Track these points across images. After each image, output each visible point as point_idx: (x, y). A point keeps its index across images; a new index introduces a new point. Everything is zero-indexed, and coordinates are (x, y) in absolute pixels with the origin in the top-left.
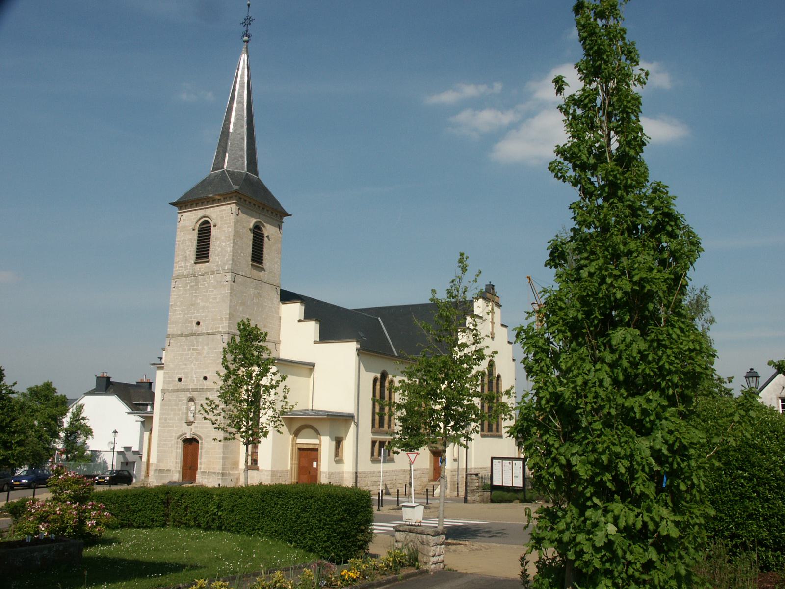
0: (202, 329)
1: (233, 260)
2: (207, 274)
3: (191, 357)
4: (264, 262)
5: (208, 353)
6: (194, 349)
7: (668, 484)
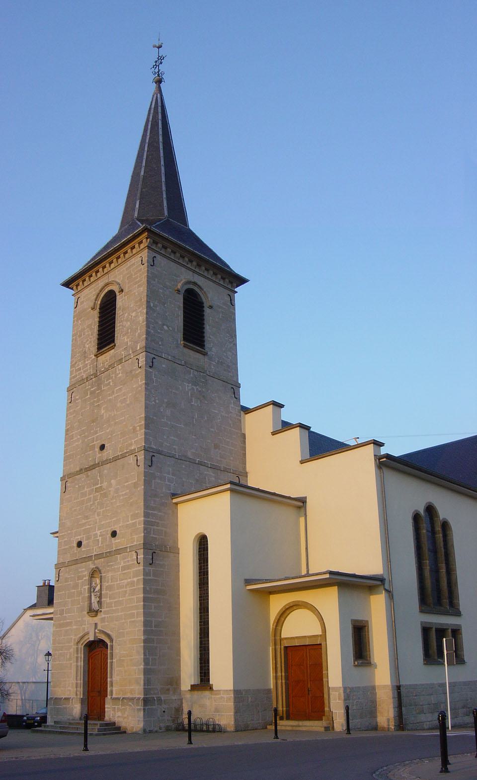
0: (108, 453)
1: (148, 333)
2: (112, 366)
3: (94, 503)
4: (207, 345)
5: (117, 491)
6: (97, 490)
7: (82, 697)
